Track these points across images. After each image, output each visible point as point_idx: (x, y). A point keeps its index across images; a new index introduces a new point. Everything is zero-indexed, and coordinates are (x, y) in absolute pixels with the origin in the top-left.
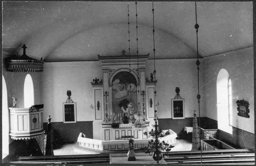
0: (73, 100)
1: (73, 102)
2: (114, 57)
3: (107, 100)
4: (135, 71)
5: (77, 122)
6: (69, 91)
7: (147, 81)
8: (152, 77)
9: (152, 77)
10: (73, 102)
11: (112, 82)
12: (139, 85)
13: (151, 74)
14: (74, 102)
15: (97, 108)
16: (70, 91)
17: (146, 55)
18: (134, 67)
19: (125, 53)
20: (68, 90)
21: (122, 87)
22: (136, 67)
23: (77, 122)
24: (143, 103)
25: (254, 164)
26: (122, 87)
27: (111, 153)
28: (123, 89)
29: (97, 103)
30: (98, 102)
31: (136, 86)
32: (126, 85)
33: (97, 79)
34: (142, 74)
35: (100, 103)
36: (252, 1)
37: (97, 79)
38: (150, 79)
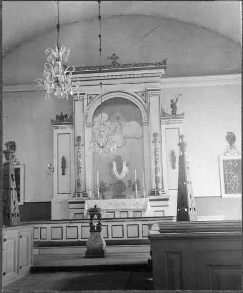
0: (19, 160)
1: (18, 164)
2: (96, 69)
3: (155, 154)
4: (138, 97)
5: (25, 203)
6: (231, 133)
7: (163, 115)
8: (173, 106)
9: (173, 106)
10: (18, 164)
11: (93, 118)
12: (148, 123)
13: (172, 101)
14: (21, 163)
15: (61, 170)
16: (14, 142)
17: (159, 63)
18: (133, 89)
19: (117, 60)
20: (229, 131)
21: (112, 129)
22: (140, 88)
23: (25, 203)
24: (155, 158)
25: (238, 244)
26: (112, 129)
27: (180, 257)
28: (115, 131)
29: (61, 161)
30: (64, 160)
31: (142, 125)
32: (120, 124)
33: (64, 114)
34: (153, 100)
35: (68, 160)
36: (2, 3)
37: (64, 114)
38: (169, 111)
